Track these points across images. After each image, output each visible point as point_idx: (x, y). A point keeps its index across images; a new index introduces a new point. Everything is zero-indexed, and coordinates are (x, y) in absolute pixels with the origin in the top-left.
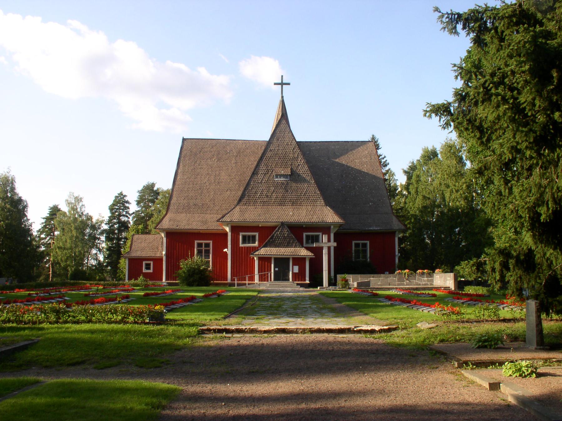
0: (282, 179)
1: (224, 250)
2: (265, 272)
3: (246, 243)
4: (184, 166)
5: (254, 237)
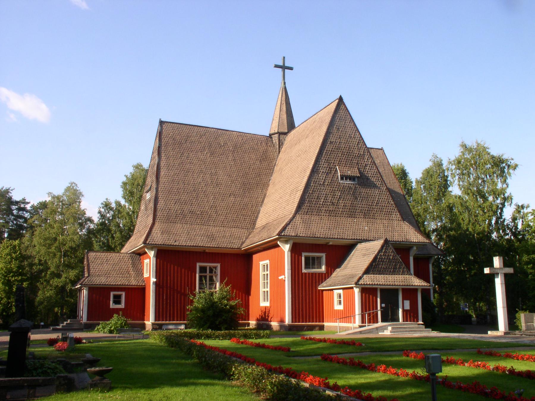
0: (348, 182)
1: (280, 278)
2: (373, 310)
3: (309, 268)
4: (168, 158)
5: (319, 258)
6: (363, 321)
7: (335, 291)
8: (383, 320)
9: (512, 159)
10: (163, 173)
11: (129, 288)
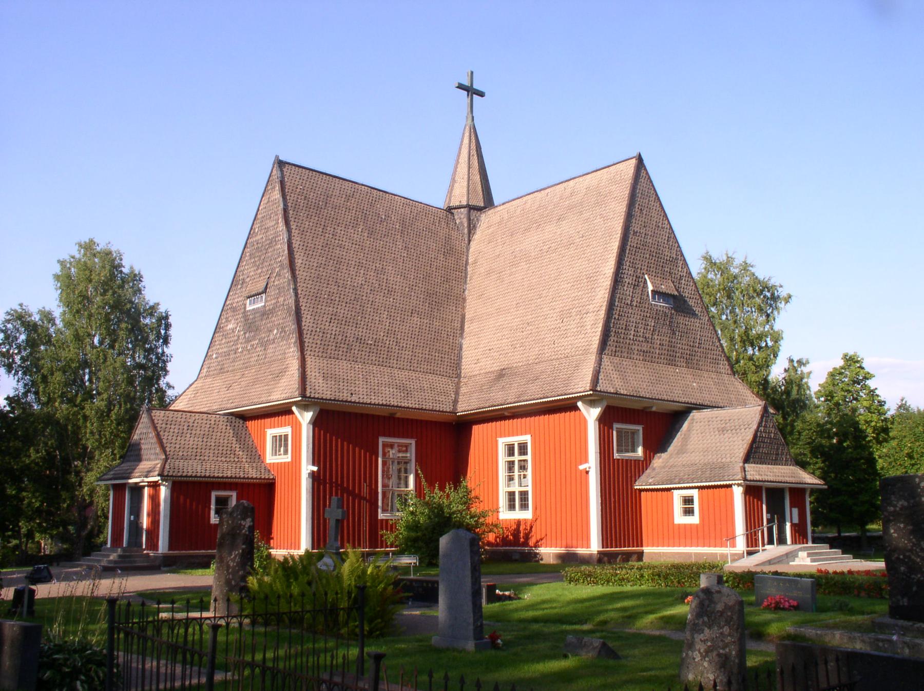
5: (634, 433)
6: (752, 541)
7: (676, 492)
8: (794, 542)
9: (781, 286)
10: (300, 261)
11: (243, 484)
